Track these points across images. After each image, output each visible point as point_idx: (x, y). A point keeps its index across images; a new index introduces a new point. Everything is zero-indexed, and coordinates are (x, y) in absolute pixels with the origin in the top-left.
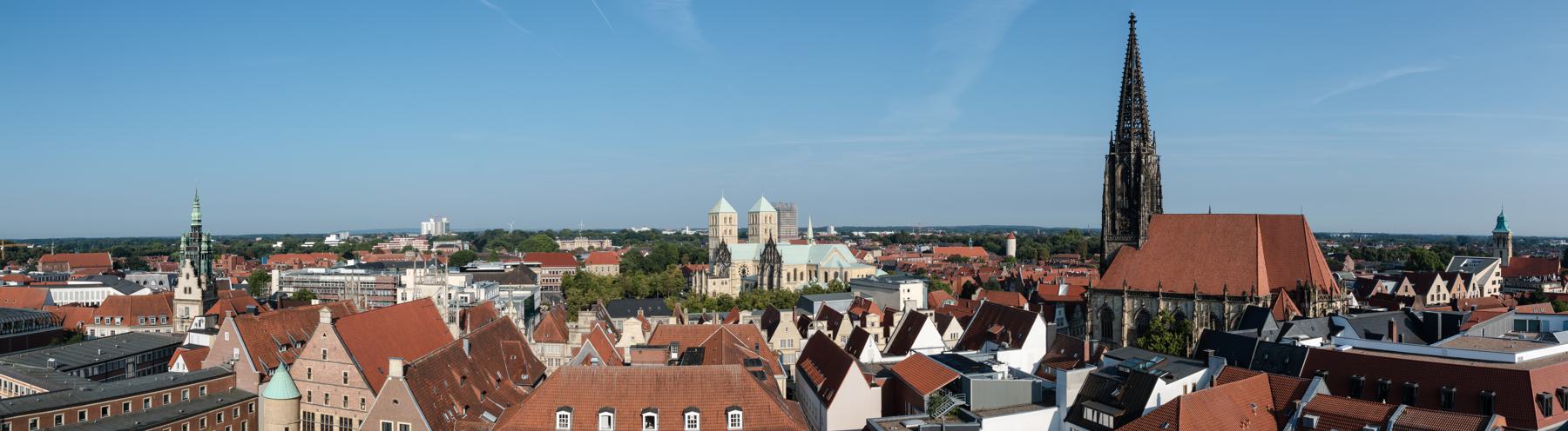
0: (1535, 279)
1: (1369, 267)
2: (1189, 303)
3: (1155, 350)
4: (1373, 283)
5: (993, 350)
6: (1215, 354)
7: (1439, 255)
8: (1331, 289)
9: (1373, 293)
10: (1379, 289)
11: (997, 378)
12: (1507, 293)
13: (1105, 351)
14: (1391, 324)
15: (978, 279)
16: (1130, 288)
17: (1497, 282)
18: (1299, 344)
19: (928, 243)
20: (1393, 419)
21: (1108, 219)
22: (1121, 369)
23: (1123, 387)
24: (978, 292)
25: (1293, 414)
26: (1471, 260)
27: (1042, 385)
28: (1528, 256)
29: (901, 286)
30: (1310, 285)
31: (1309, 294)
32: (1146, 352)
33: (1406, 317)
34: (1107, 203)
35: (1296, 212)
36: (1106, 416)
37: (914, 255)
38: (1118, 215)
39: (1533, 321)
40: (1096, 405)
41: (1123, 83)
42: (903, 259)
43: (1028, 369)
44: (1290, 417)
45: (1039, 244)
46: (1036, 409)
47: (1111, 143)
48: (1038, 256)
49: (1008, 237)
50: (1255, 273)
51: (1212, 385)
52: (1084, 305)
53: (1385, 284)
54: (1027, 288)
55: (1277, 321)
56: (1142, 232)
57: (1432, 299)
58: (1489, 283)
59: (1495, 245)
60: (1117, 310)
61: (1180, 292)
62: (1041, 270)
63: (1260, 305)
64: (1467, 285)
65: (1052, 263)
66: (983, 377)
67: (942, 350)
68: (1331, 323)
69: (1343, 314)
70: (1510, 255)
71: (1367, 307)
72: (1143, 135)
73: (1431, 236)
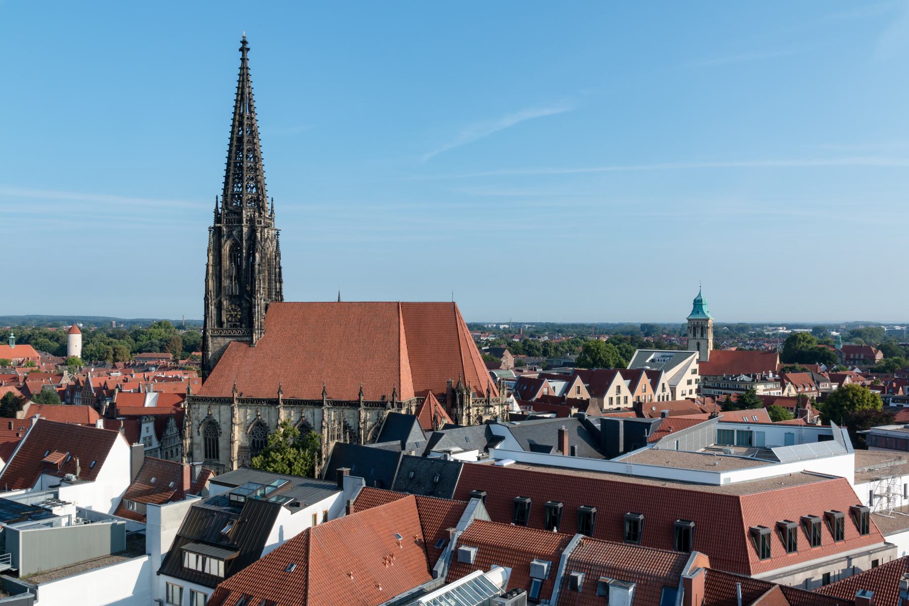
1: (532, 364)
3: (275, 471)
4: (537, 383)
6: (351, 473)
7: (620, 348)
8: (488, 391)
9: (538, 395)
10: (545, 390)
11: (59, 524)
12: (707, 396)
13: (211, 476)
14: (561, 433)
15: (24, 389)
16: (241, 394)
17: (693, 382)
18: (451, 458)
20: (567, 553)
21: (212, 308)
22: (233, 498)
23: (236, 521)
24: (26, 407)
25: (446, 545)
26: (659, 355)
27: (126, 528)
28: (734, 349)
30: (463, 386)
31: (462, 397)
32: (264, 474)
33: (580, 424)
34: (211, 288)
35: (447, 299)
36: (214, 562)
39: (743, 431)
40: (200, 547)
41: (232, 132)
43: (104, 507)
44: (442, 550)
45: (114, 340)
46: (118, 562)
48: (114, 355)
49: (70, 331)
51: (348, 512)
52: (180, 418)
53: (552, 384)
55: (425, 431)
56: (256, 325)
57: (611, 403)
58: (684, 381)
59: (691, 336)
60: (225, 423)
62: (119, 374)
63: (403, 412)
64: (654, 385)
65: (134, 365)
66: (38, 526)
68: (488, 432)
70: (711, 347)
71: (531, 413)
72: (258, 203)
73: (607, 324)
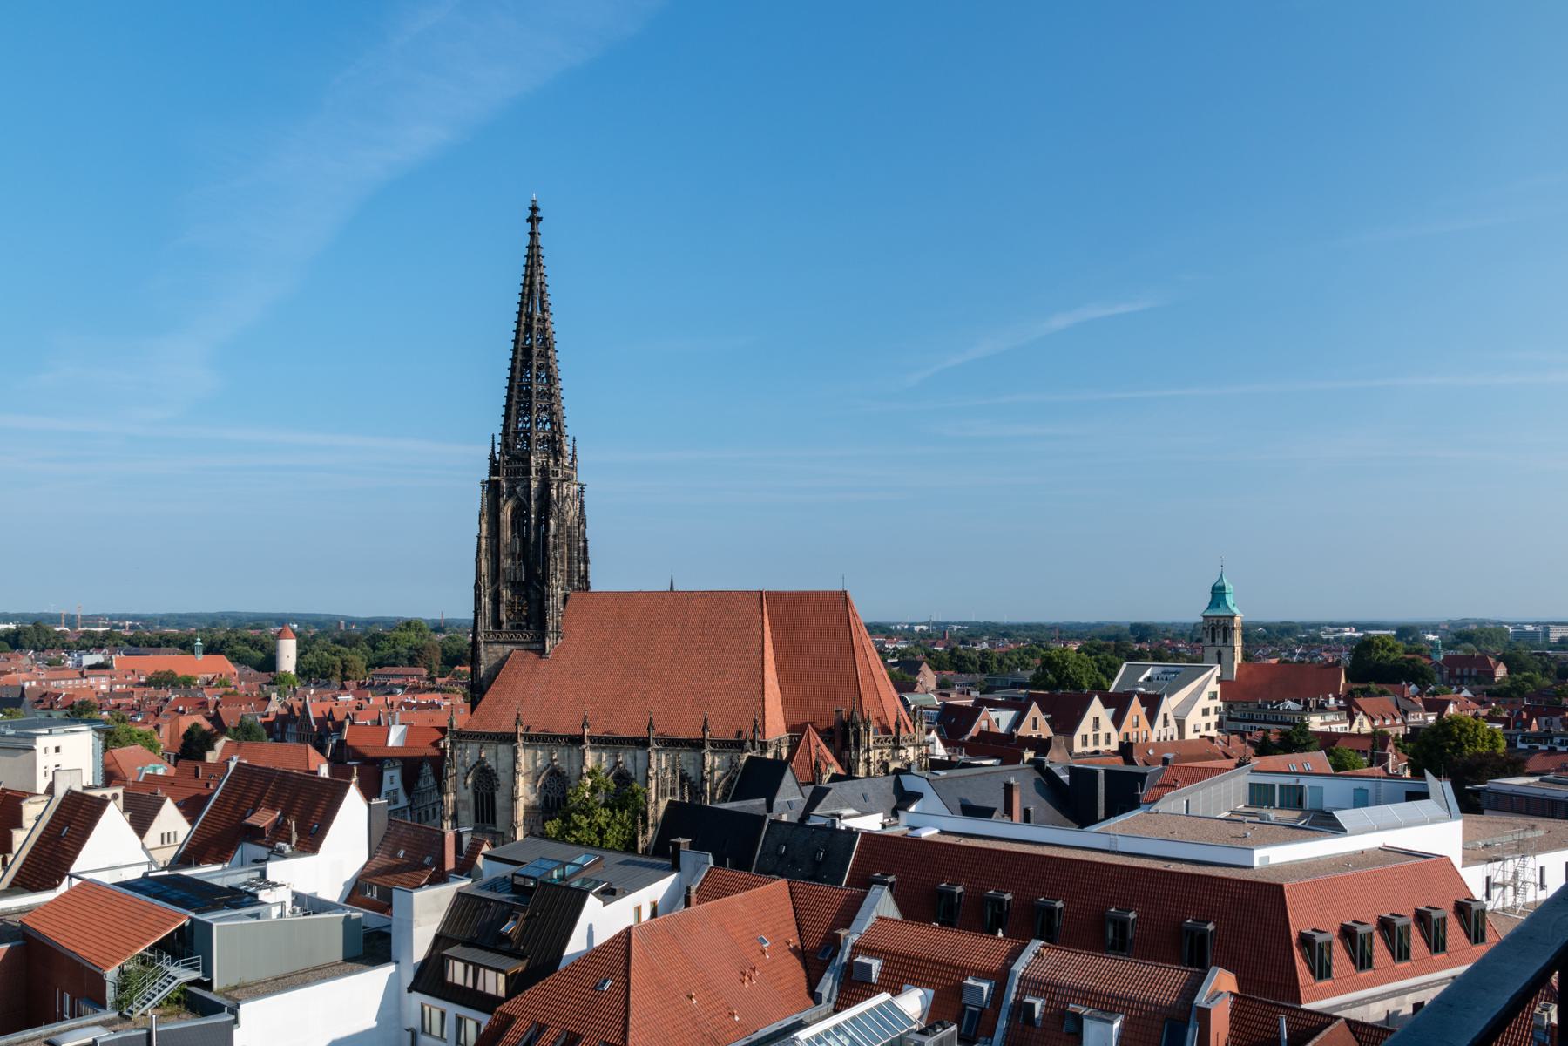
0: (1290, 704)
2: (640, 754)
3: (578, 843)
4: (972, 714)
5: (256, 861)
6: (692, 846)
7: (1097, 660)
8: (897, 725)
9: (973, 732)
10: (984, 724)
11: (268, 915)
12: (1233, 732)
13: (485, 849)
14: (1009, 789)
15: (216, 719)
16: (528, 728)
17: (1212, 711)
18: (842, 825)
19: (101, 647)
20: (1019, 968)
21: (486, 600)
22: (519, 881)
23: (522, 915)
24: (220, 744)
25: (835, 955)
26: (1159, 670)
28: (1274, 661)
29: (38, 739)
31: (857, 734)
32: (563, 846)
34: (484, 570)
36: (491, 975)
37: (65, 674)
38: (506, 594)
39: (1289, 787)
41: (516, 341)
42: (39, 682)
43: (332, 892)
45: (343, 648)
46: (352, 972)
47: (492, 458)
48: (343, 671)
49: (279, 635)
50: (759, 698)
51: (687, 904)
52: (438, 764)
54: (323, 734)
56: (551, 625)
57: (1085, 743)
58: (1196, 711)
59: (1207, 641)
60: (504, 771)
61: (622, 733)
62: (350, 698)
63: (769, 755)
65: (371, 685)
66: (238, 917)
67: (145, 869)
69: (920, 769)
70: (1239, 659)
72: (554, 445)
